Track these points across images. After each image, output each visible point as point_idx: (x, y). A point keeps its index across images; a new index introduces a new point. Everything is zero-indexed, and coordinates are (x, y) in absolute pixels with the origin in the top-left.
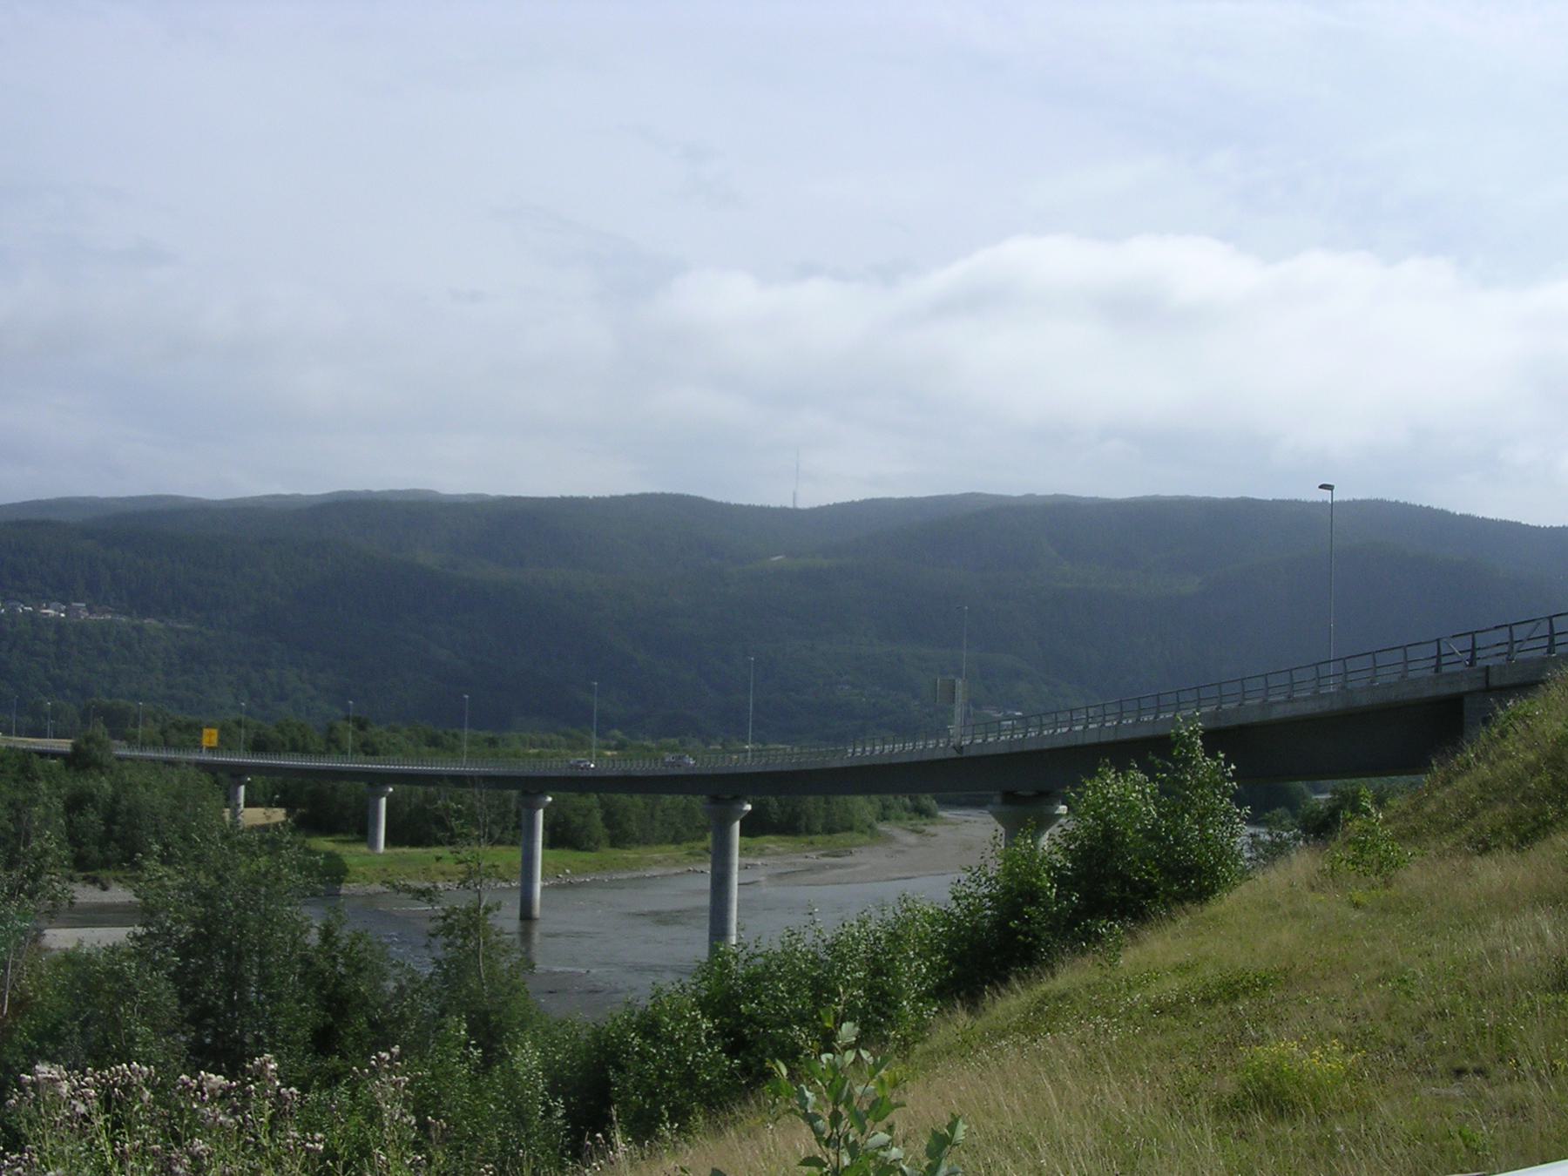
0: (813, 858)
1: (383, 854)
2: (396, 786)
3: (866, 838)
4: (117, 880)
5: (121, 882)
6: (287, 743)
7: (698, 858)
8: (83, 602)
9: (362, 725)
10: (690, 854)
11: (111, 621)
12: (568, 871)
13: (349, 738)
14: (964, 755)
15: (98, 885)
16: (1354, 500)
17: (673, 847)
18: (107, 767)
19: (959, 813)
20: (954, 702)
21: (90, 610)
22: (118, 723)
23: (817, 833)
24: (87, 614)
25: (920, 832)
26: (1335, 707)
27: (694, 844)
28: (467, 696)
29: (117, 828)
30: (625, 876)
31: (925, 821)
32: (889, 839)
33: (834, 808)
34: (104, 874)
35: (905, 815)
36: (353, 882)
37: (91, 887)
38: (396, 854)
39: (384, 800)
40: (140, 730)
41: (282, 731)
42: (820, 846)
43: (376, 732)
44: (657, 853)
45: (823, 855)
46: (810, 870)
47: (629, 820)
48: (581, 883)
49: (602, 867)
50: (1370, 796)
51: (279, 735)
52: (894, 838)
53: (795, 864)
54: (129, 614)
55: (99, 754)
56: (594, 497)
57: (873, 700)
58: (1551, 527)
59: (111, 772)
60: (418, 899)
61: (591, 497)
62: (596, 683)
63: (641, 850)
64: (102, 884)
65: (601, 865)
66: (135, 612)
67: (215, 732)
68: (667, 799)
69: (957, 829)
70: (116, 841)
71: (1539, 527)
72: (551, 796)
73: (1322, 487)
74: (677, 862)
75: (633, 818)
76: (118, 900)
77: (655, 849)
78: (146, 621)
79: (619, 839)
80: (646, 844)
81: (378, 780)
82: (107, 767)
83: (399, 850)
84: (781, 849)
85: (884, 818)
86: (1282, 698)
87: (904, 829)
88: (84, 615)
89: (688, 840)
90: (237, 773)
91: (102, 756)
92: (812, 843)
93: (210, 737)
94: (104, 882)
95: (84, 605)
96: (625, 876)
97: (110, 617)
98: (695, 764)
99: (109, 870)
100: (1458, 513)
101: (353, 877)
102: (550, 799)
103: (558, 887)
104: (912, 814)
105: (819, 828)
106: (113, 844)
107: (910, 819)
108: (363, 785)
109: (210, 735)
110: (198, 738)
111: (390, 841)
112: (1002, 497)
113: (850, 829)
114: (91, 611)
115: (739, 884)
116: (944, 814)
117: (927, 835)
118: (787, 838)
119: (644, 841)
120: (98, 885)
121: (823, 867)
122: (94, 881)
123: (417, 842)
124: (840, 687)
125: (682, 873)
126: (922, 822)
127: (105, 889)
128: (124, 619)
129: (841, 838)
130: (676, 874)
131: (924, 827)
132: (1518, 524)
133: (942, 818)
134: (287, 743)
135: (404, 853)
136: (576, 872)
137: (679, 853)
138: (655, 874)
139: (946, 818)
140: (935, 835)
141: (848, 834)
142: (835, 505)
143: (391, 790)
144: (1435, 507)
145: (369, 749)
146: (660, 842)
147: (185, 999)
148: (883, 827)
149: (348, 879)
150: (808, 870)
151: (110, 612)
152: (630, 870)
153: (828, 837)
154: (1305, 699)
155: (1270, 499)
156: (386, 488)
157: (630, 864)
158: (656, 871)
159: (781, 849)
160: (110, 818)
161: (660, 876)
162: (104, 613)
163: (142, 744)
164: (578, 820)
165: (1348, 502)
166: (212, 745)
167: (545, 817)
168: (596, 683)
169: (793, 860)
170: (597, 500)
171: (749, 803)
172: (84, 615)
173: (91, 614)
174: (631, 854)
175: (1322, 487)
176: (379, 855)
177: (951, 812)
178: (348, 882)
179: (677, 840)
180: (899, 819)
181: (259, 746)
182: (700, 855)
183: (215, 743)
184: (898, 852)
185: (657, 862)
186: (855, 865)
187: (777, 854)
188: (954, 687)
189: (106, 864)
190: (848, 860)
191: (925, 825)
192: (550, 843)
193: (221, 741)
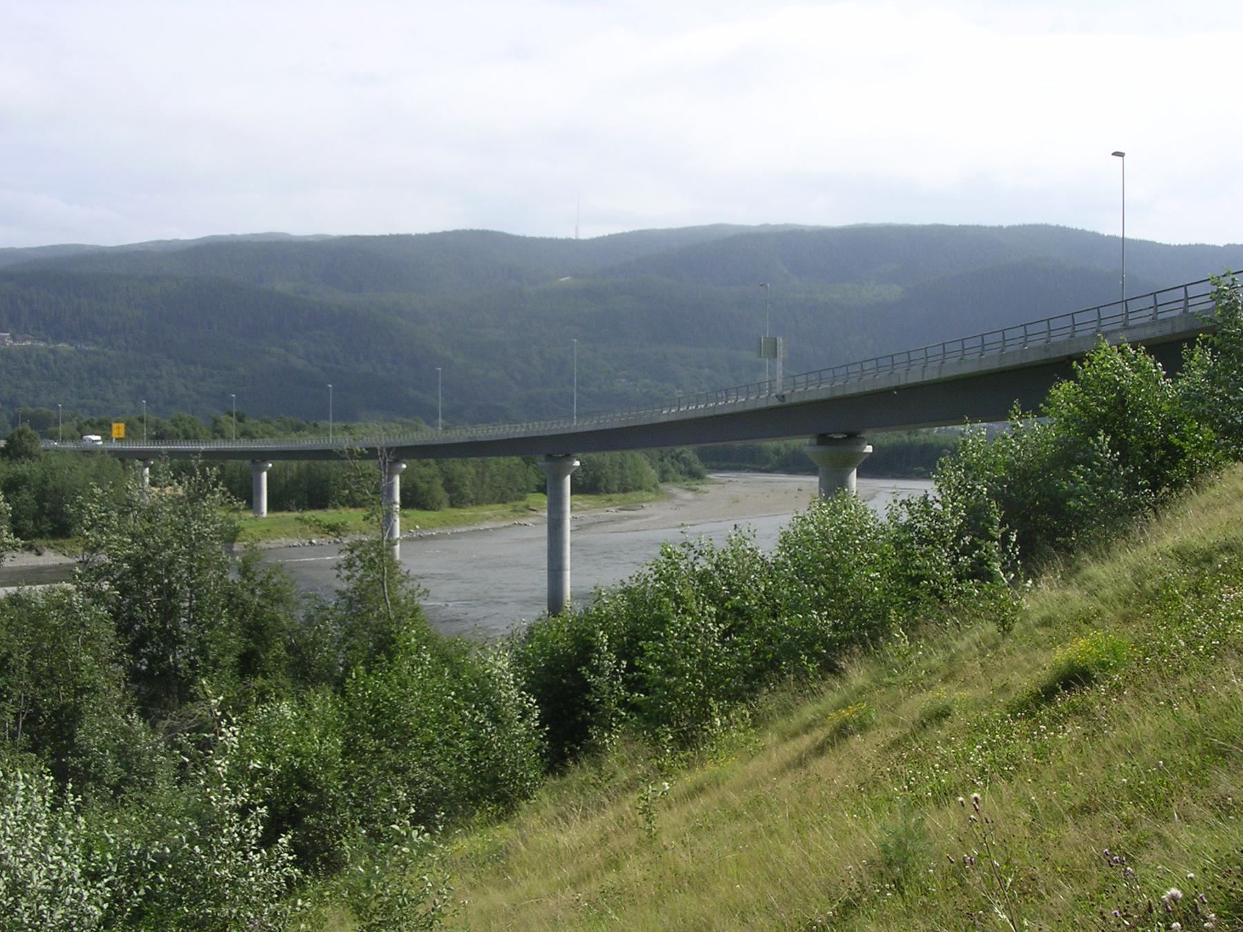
0: (613, 512)
1: (267, 518)
2: (275, 462)
3: (651, 496)
4: (49, 547)
5: (52, 548)
6: (181, 434)
7: (521, 514)
8: (7, 332)
9: (240, 419)
10: (515, 511)
11: (30, 347)
12: (417, 527)
13: (232, 427)
14: (785, 403)
15: (34, 551)
16: (1024, 225)
17: (500, 506)
18: (37, 456)
19: (722, 475)
20: (776, 357)
21: (13, 338)
22: (43, 425)
23: (614, 492)
24: (12, 342)
25: (695, 490)
26: (1178, 330)
27: (517, 503)
28: (330, 386)
29: (47, 504)
30: (464, 529)
31: (698, 482)
32: (671, 497)
33: (627, 471)
34: (37, 542)
35: (680, 477)
36: (243, 541)
37: (28, 552)
38: (278, 517)
39: (265, 475)
40: (61, 428)
41: (176, 425)
42: (617, 502)
43: (250, 421)
44: (486, 511)
45: (620, 509)
46: (612, 521)
47: (464, 485)
48: (429, 536)
49: (445, 523)
50: (384, 659)
51: (174, 428)
52: (675, 495)
53: (599, 517)
54: (45, 340)
55: (29, 444)
56: (416, 235)
57: (645, 390)
58: (1179, 245)
59: (40, 459)
60: (328, 534)
61: (413, 234)
62: (440, 369)
63: (475, 509)
64: (37, 551)
65: (444, 522)
66: (50, 338)
67: (122, 425)
68: (505, 461)
69: (724, 487)
70: (48, 515)
71: (1170, 245)
72: (405, 463)
73: (1115, 154)
74: (504, 517)
75: (467, 483)
76: (51, 563)
77: (485, 507)
78: (60, 345)
79: (457, 500)
80: (478, 504)
81: (260, 457)
82: (37, 456)
83: (279, 514)
84: (586, 506)
85: (664, 479)
86: (1118, 326)
87: (680, 488)
88: (9, 342)
89: (511, 500)
90: (144, 456)
91: (31, 447)
92: (610, 500)
93: (118, 430)
94: (39, 549)
95: (8, 334)
96: (464, 529)
97: (30, 343)
98: (135, 630)
99: (42, 538)
100: (1106, 235)
101: (244, 537)
102: (404, 466)
103: (409, 540)
104: (686, 477)
105: (616, 487)
106: (45, 518)
107: (684, 481)
108: (247, 463)
109: (119, 428)
110: (108, 433)
111: (274, 505)
112: (742, 227)
113: (640, 488)
114: (15, 340)
115: (571, 531)
116: (711, 476)
117: (700, 492)
118: (591, 496)
119: (477, 502)
120: (34, 551)
121: (621, 519)
122: (30, 548)
123: (281, 509)
124: (617, 380)
125: (509, 527)
126: (694, 483)
127: (39, 554)
128: (42, 344)
129: (632, 496)
130: (505, 526)
131: (697, 487)
132: (1153, 243)
133: (709, 478)
134: (181, 434)
135: (283, 516)
136: (423, 528)
137: (505, 510)
138: (488, 527)
139: (712, 479)
140: (707, 492)
141: (639, 492)
142: (610, 235)
143: (270, 465)
144: (1088, 230)
145: (245, 434)
146: (490, 502)
147: (123, 630)
148: (662, 486)
149: (239, 539)
150: (611, 521)
151: (29, 339)
152: (468, 525)
153: (622, 495)
154: (1144, 325)
155: (957, 225)
156: (248, 232)
157: (467, 521)
158: (488, 525)
159: (586, 506)
160: (40, 499)
161: (493, 529)
162: (24, 341)
163: (63, 439)
164: (423, 486)
165: (1020, 226)
166: (121, 436)
167: (401, 482)
168: (440, 369)
169: (599, 514)
170: (419, 237)
171: (578, 460)
172: (9, 342)
173: (14, 341)
174: (467, 512)
175: (1115, 154)
176: (263, 519)
177: (718, 475)
178: (239, 541)
179: (503, 500)
180: (675, 480)
181: (159, 437)
182: (522, 512)
183: (122, 435)
184: (678, 505)
185: (488, 518)
186: (647, 516)
187: (584, 509)
188: (776, 344)
189: (40, 534)
190: (641, 512)
191: (697, 484)
192: (405, 504)
193: (127, 433)
